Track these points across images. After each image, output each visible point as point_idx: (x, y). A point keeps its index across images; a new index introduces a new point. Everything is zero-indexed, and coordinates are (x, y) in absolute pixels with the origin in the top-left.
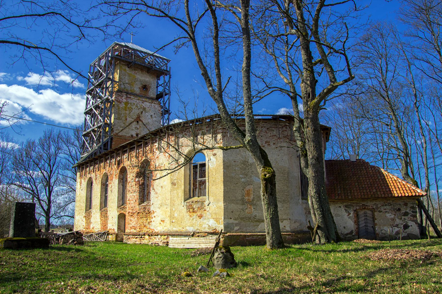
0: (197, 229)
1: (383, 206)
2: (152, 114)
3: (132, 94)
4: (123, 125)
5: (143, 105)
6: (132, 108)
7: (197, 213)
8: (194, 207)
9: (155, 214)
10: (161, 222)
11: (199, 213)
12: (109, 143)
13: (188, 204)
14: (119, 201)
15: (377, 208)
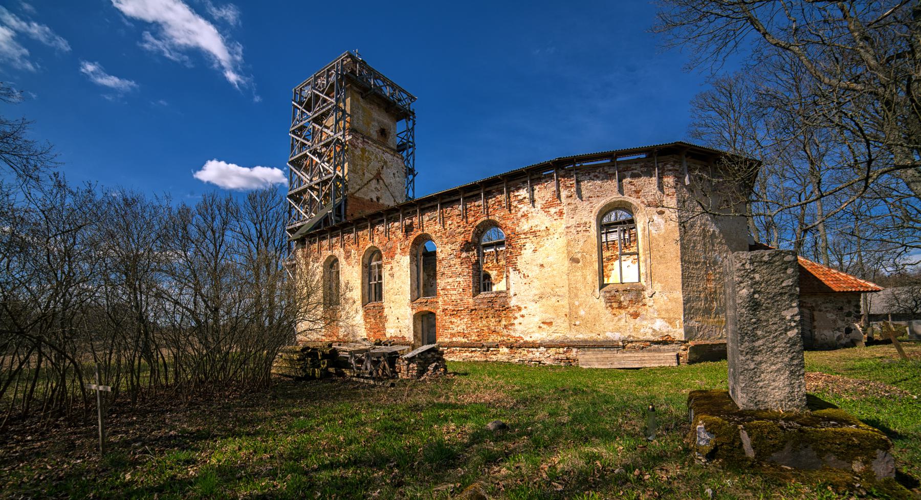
0: (630, 336)
1: (823, 303)
2: (395, 172)
3: (368, 138)
4: (360, 182)
5: (384, 156)
6: (371, 159)
7: (628, 310)
8: (622, 299)
9: (523, 312)
10: (542, 325)
11: (632, 310)
12: (343, 207)
13: (608, 295)
14: (412, 291)
15: (817, 305)
